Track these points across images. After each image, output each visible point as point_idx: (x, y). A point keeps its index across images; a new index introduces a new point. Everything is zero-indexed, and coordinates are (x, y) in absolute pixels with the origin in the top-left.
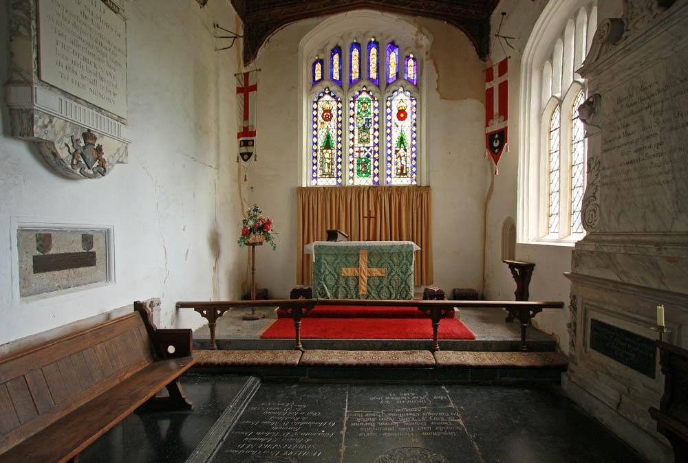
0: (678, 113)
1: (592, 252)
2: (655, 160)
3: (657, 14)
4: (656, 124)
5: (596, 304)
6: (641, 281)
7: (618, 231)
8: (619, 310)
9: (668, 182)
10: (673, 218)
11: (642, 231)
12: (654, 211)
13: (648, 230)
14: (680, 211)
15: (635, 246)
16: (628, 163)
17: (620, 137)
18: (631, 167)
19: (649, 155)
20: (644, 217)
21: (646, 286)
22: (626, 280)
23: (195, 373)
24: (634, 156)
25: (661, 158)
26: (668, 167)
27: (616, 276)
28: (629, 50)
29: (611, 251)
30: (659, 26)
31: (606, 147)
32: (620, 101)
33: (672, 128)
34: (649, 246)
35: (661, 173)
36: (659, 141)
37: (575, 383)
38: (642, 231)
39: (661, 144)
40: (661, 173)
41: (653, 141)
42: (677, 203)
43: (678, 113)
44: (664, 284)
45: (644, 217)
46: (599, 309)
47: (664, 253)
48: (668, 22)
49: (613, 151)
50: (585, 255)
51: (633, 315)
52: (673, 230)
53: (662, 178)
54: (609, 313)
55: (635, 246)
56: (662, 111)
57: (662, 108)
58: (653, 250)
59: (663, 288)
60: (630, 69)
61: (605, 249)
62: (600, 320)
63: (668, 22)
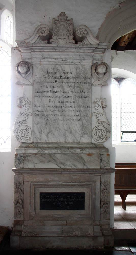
0: (83, 91)
1: (36, 154)
2: (71, 109)
3: (72, 42)
4: (71, 92)
5: (42, 184)
6: (73, 166)
7: (47, 142)
8: (60, 183)
9: (78, 120)
10: (81, 137)
11: (72, 142)
12: (71, 132)
13: (67, 141)
14: (84, 133)
15: (67, 149)
16: (54, 107)
17: (48, 92)
18: (55, 109)
19: (67, 105)
20: (65, 135)
21: (76, 168)
22: (63, 167)
23: (50, 32)
24: (58, 104)
25: (74, 109)
26: (78, 113)
27: (56, 166)
28: (56, 49)
29: (51, 152)
30: (75, 48)
31: (37, 94)
32: (48, 73)
33: (80, 97)
34: (76, 149)
35: (74, 116)
36: (73, 100)
37: (26, 236)
38: (64, 142)
39: (74, 102)
40: (74, 116)
41: (69, 99)
42: (83, 130)
43: (83, 91)
44: (86, 166)
45: (65, 135)
46: (41, 186)
47: (84, 152)
48: (79, 49)
49: (43, 98)
50: (29, 156)
51: (69, 184)
52: (80, 142)
53: (75, 118)
54: (55, 186)
55: (67, 149)
56: (74, 87)
57: (74, 85)
58: (78, 151)
59: (85, 167)
60: (56, 59)
61: (46, 152)
62: (46, 191)
63: (79, 49)
